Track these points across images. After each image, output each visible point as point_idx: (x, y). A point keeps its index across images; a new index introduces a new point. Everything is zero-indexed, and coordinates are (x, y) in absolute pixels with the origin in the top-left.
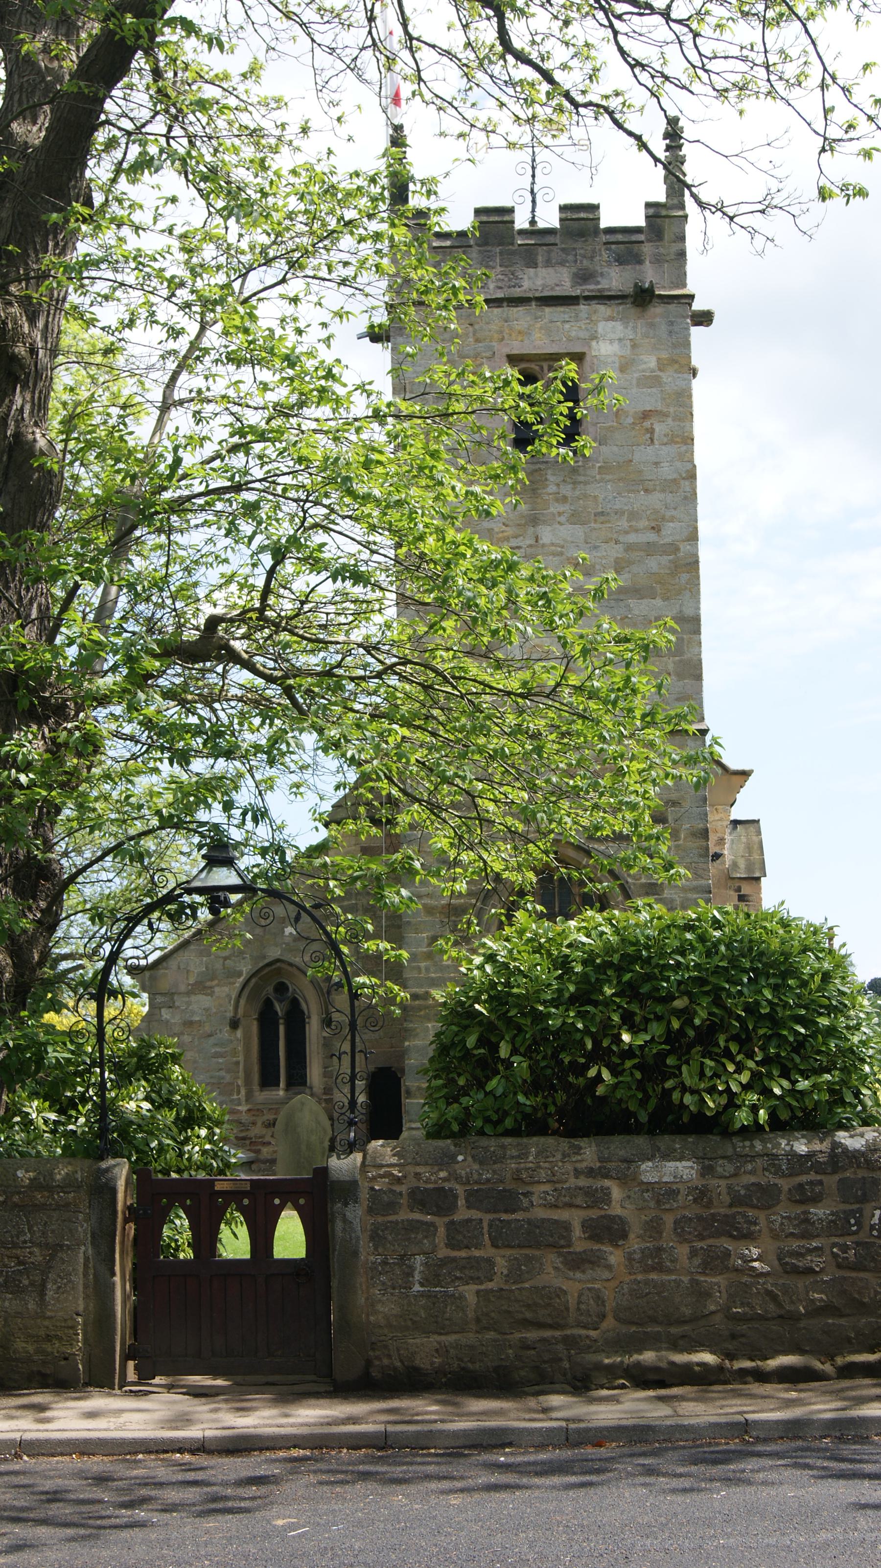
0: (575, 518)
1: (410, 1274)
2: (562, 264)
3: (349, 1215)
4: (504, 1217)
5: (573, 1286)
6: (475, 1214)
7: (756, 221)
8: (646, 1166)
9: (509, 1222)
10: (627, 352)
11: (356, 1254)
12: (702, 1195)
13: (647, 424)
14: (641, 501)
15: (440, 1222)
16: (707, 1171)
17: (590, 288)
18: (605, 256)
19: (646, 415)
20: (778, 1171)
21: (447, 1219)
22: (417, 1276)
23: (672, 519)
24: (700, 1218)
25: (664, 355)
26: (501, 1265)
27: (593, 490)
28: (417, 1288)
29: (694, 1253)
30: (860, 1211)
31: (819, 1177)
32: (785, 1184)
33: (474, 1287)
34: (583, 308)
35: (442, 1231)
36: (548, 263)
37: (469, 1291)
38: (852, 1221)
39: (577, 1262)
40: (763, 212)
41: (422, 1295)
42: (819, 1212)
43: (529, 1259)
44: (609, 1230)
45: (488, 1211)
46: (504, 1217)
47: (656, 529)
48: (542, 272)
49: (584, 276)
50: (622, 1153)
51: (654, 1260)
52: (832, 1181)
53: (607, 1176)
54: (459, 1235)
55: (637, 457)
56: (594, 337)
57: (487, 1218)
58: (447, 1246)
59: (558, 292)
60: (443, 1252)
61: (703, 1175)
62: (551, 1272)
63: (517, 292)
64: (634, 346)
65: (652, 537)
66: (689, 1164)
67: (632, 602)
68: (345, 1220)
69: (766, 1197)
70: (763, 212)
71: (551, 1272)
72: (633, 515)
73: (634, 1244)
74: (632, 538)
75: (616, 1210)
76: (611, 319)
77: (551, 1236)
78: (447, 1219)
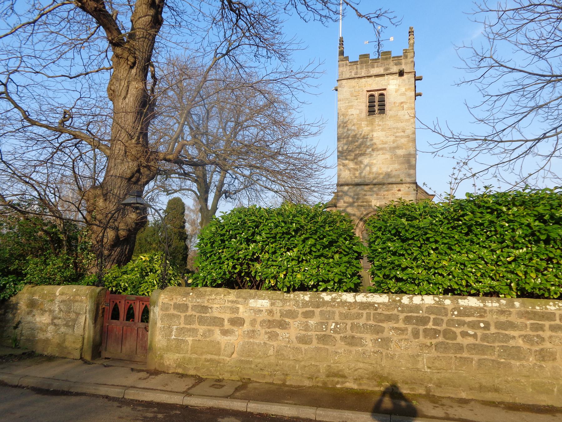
0: (383, 130)
1: (171, 332)
2: (381, 67)
3: (155, 311)
4: (203, 315)
5: (223, 340)
6: (194, 313)
7: (375, 20)
8: (252, 301)
9: (205, 317)
10: (397, 87)
11: (156, 323)
12: (270, 312)
13: (402, 105)
14: (400, 125)
15: (183, 315)
16: (272, 304)
17: (389, 72)
18: (392, 63)
19: (402, 103)
20: (298, 306)
21: (185, 314)
22: (173, 333)
23: (408, 129)
24: (269, 321)
25: (407, 87)
26: (201, 332)
27: (387, 123)
28: (173, 337)
29: (266, 333)
30: (327, 323)
31: (313, 309)
32: (301, 311)
33: (191, 338)
34: (386, 77)
35: (183, 318)
36: (377, 67)
37: (190, 339)
38: (324, 327)
39: (225, 333)
40: (377, 17)
41: (174, 339)
42: (312, 322)
43: (209, 331)
44: (237, 322)
45: (198, 313)
46: (203, 315)
47: (404, 132)
48: (376, 69)
49: (386, 69)
50: (244, 296)
51: (252, 333)
52: (317, 311)
53: (238, 303)
54: (189, 320)
55: (399, 114)
56: (389, 84)
57: (198, 315)
58: (184, 323)
59: (380, 73)
60: (182, 326)
61: (271, 306)
62: (217, 335)
63: (369, 74)
64: (399, 86)
65: (402, 134)
66: (267, 301)
67: (397, 151)
68: (154, 312)
69: (292, 314)
70: (377, 17)
71: (217, 335)
72: (397, 129)
73: (247, 327)
74: (397, 134)
75: (241, 315)
76: (393, 79)
77: (218, 322)
78: (185, 314)
